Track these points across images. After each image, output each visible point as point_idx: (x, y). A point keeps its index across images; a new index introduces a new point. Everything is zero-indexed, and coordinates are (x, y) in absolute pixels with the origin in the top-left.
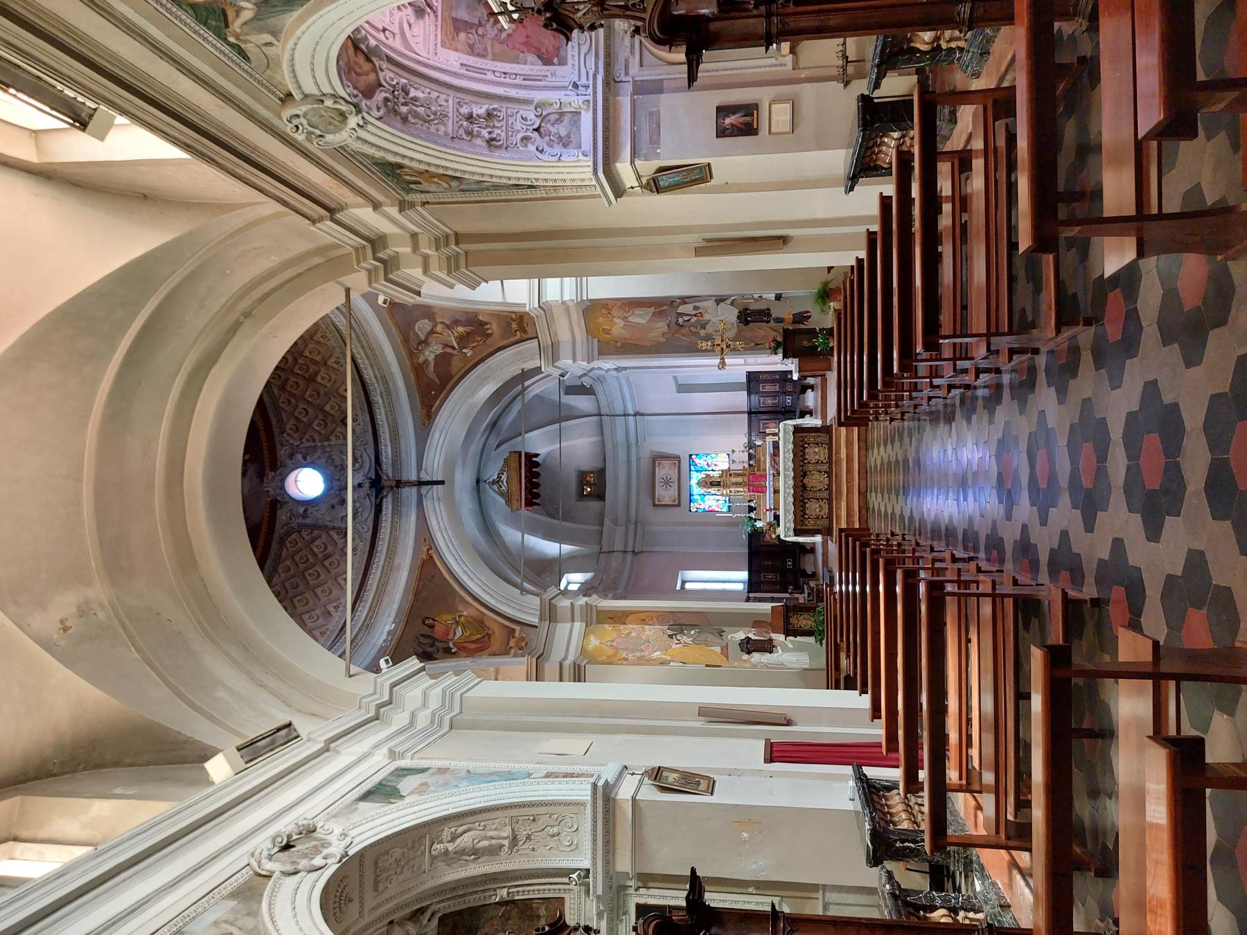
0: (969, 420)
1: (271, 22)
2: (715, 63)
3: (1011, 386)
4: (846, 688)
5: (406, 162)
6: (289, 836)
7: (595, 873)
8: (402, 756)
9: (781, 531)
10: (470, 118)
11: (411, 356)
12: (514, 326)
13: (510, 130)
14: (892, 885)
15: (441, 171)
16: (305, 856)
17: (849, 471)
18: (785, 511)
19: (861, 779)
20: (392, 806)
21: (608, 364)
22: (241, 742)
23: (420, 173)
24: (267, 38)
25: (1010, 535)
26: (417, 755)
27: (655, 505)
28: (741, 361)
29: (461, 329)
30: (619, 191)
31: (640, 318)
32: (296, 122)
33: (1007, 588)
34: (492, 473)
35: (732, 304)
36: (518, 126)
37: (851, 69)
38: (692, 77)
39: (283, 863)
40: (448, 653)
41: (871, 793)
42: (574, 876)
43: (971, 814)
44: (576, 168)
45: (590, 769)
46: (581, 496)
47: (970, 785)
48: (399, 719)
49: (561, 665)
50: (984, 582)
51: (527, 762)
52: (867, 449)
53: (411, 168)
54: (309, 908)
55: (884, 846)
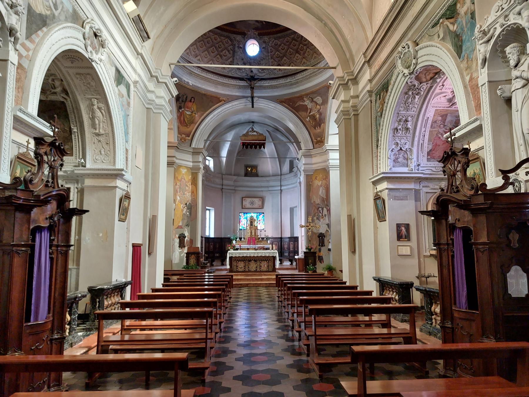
0: (278, 328)
1: (448, 38)
2: (427, 222)
3: (293, 346)
4: (164, 278)
5: (389, 93)
6: (100, 36)
7: (84, 170)
8: (135, 86)
9: (231, 251)
10: (406, 121)
11: (307, 95)
12: (319, 139)
13: (401, 138)
14: (80, 297)
15: (384, 108)
16: (92, 43)
17: (257, 280)
18: (240, 253)
19: (126, 284)
20: (113, 82)
21: (302, 178)
22: (142, 16)
23: (384, 100)
24: (442, 36)
25: (231, 346)
26: (135, 93)
27: (242, 198)
28: (303, 234)
29: (318, 116)
30: (375, 183)
31: (322, 192)
32: (406, 47)
33: (209, 345)
34: (257, 128)
35: (327, 230)
36: (403, 141)
37: (424, 279)
38: (422, 213)
39: (89, 33)
40: (179, 108)
41: (120, 289)
42: (83, 161)
43: (112, 330)
44: (385, 165)
45: (129, 168)
46: (247, 167)
47: (124, 330)
48: (151, 86)
49: (174, 157)
50: (212, 335)
51: (132, 141)
52: (266, 287)
53: (386, 96)
54: (69, 44)
55: (97, 294)
